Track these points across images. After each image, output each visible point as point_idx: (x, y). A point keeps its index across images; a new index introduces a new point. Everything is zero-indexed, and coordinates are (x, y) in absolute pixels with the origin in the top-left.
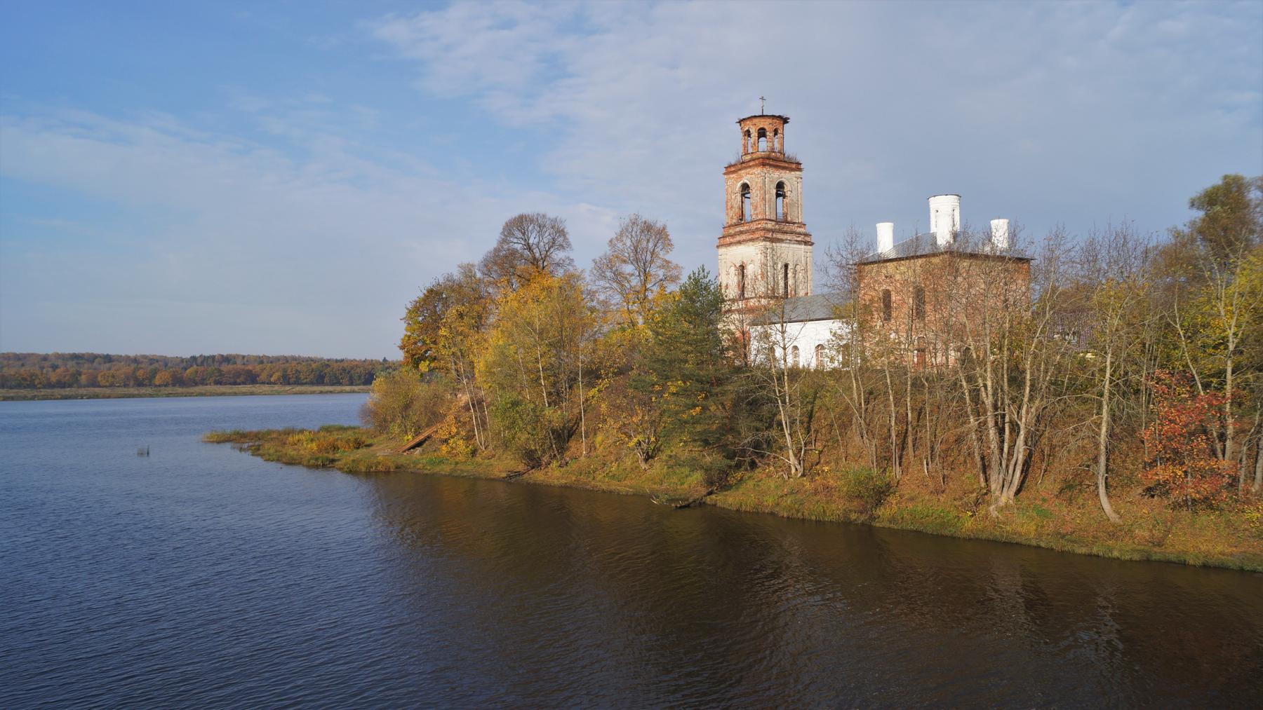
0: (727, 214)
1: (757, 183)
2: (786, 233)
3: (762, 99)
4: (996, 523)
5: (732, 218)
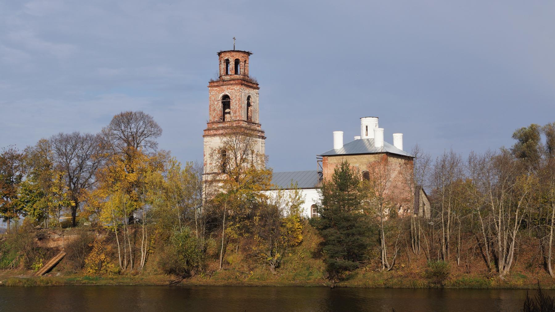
1: (236, 96)
2: (252, 130)
3: (234, 38)
4: (505, 282)
5: (215, 117)
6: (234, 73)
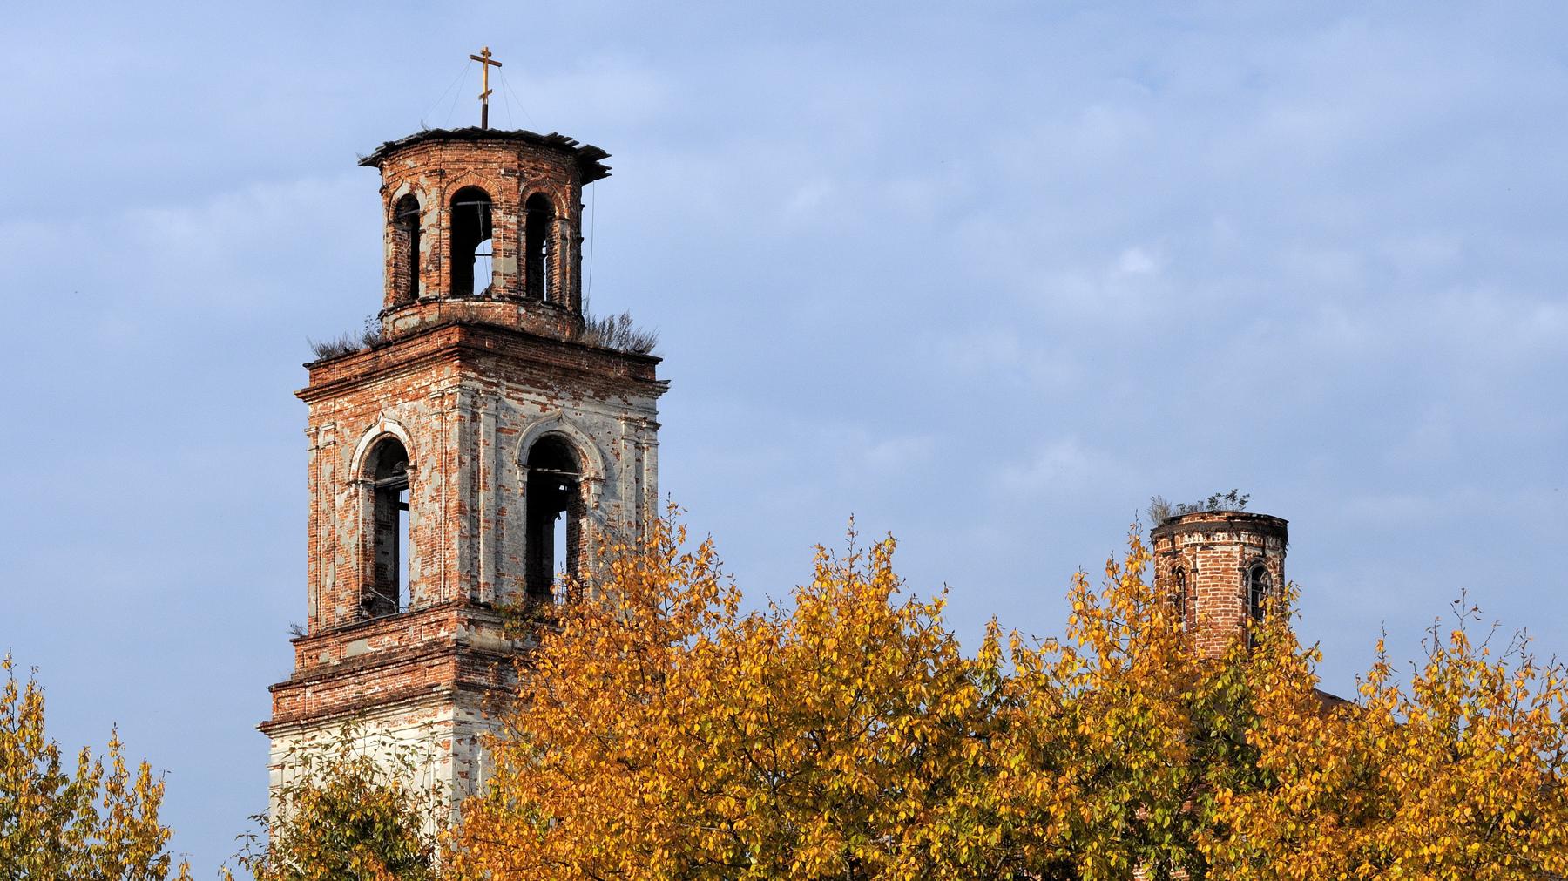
0: (316, 580)
3: (485, 59)
6: (445, 289)
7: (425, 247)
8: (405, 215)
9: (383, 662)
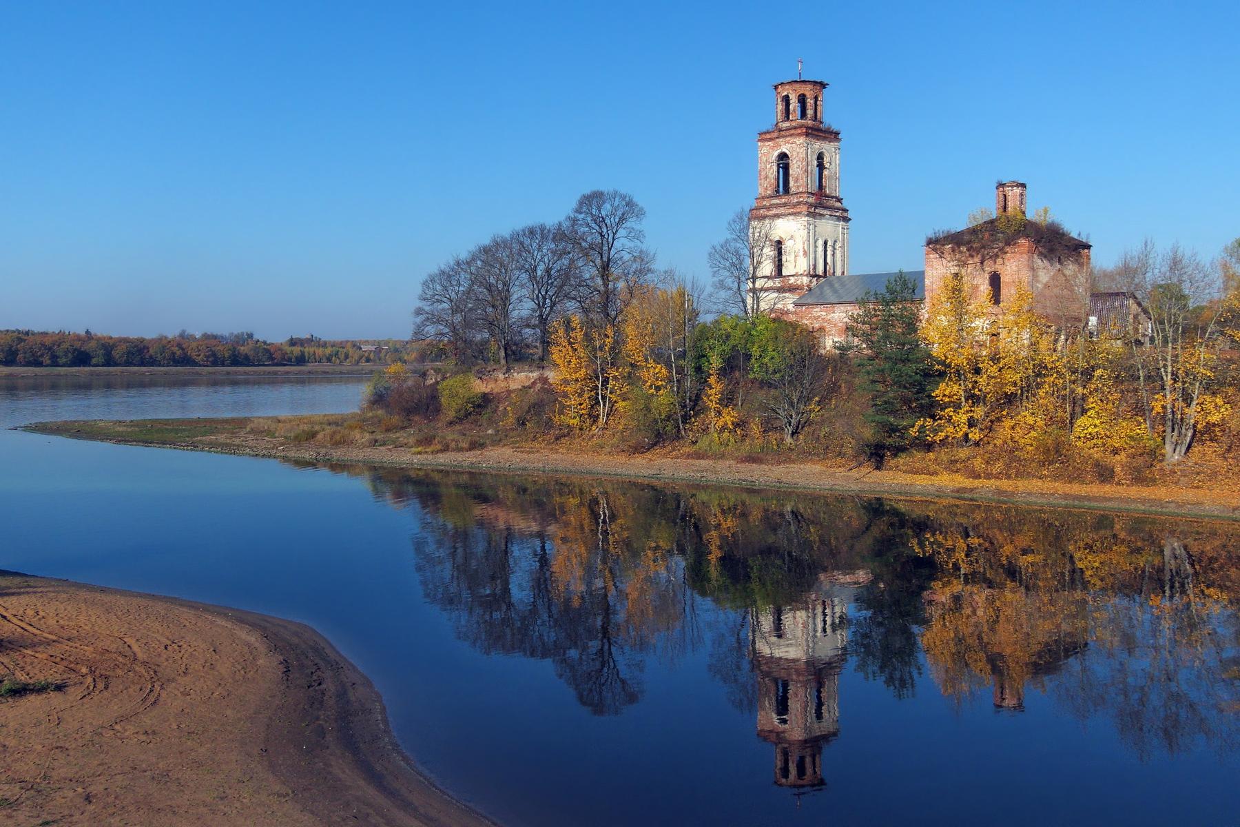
5: (766, 189)
7: (791, 107)
8: (786, 100)
9: (785, 205)
